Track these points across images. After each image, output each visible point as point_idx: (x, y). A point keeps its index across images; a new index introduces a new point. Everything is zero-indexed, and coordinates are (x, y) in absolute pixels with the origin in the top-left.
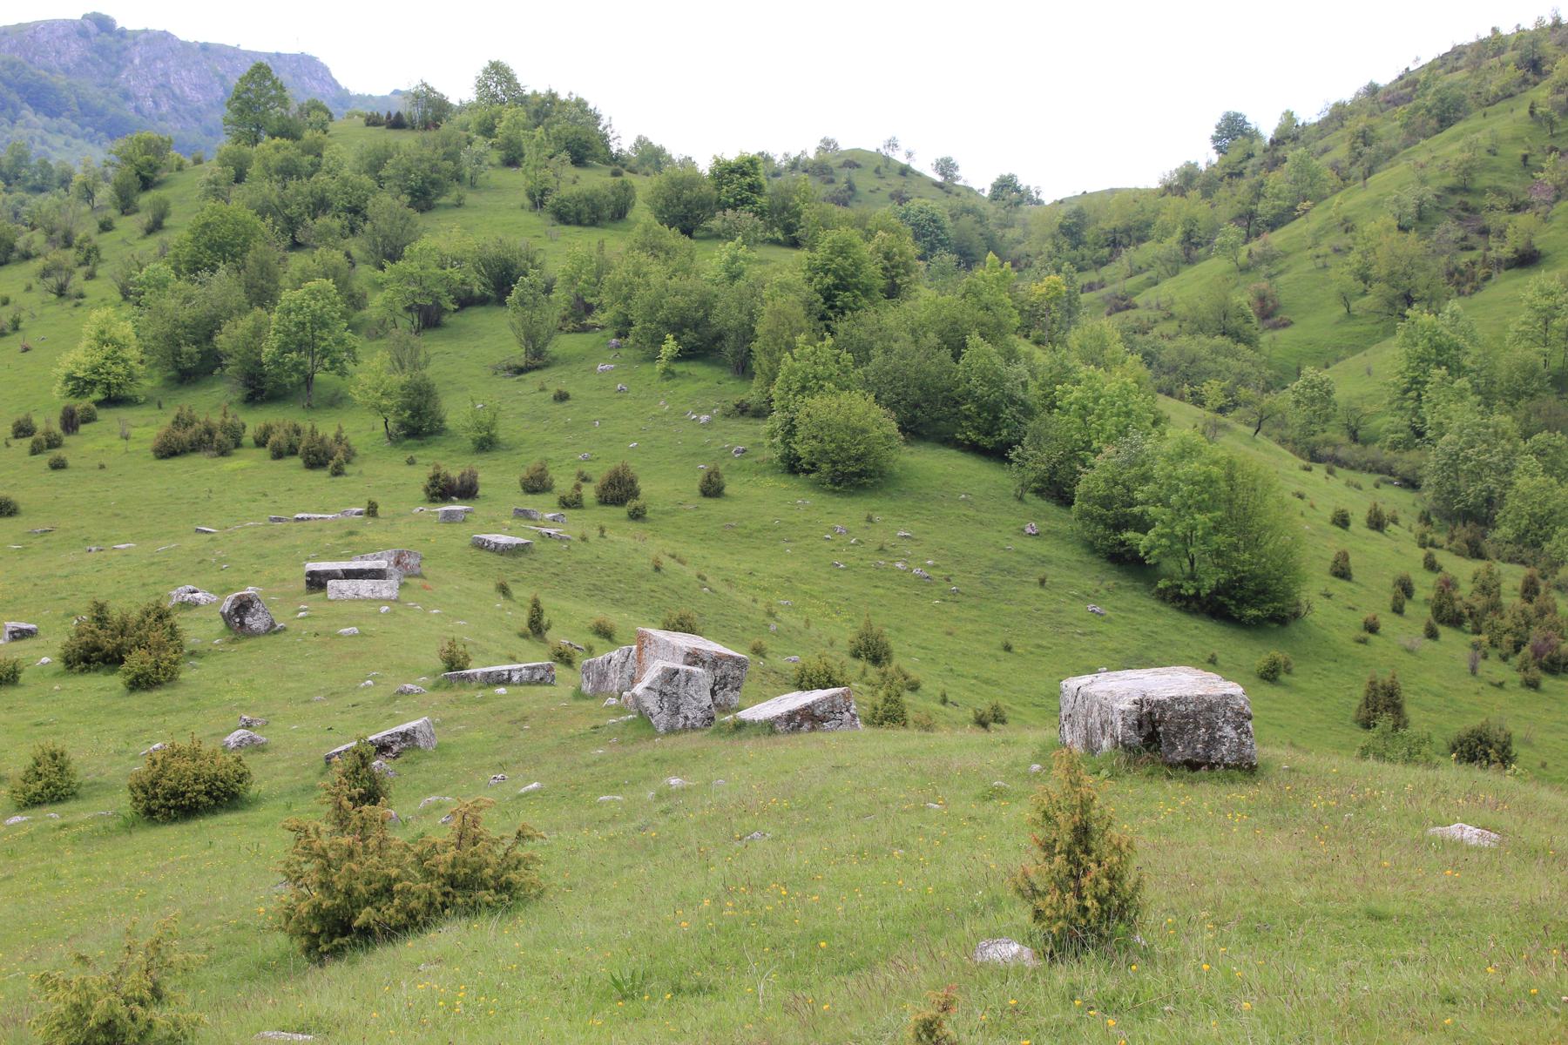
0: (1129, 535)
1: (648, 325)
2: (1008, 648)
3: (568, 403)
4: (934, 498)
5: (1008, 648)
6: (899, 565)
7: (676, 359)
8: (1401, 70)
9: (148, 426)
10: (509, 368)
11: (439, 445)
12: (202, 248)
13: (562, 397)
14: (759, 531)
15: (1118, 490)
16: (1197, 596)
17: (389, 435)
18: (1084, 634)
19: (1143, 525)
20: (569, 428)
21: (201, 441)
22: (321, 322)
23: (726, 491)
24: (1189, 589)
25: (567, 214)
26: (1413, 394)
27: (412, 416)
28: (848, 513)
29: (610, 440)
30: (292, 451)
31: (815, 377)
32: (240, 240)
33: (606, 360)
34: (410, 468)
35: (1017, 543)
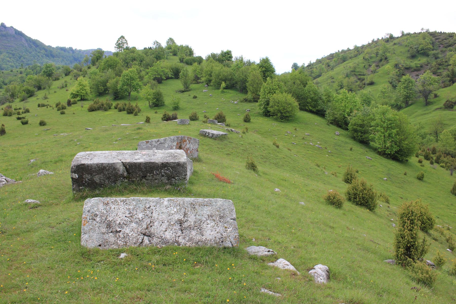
1: (217, 80)
3: (197, 99)
4: (309, 124)
7: (224, 88)
8: (322, 57)
9: (87, 105)
10: (180, 91)
11: (163, 109)
12: (106, 66)
13: (195, 97)
14: (265, 132)
17: (150, 106)
18: (371, 166)
20: (198, 105)
21: (100, 107)
22: (132, 79)
23: (251, 120)
24: (388, 151)
25: (188, 63)
27: (156, 101)
28: (288, 128)
29: (211, 107)
30: (124, 110)
31: (273, 89)
32: (115, 65)
33: (205, 89)
34: (156, 114)
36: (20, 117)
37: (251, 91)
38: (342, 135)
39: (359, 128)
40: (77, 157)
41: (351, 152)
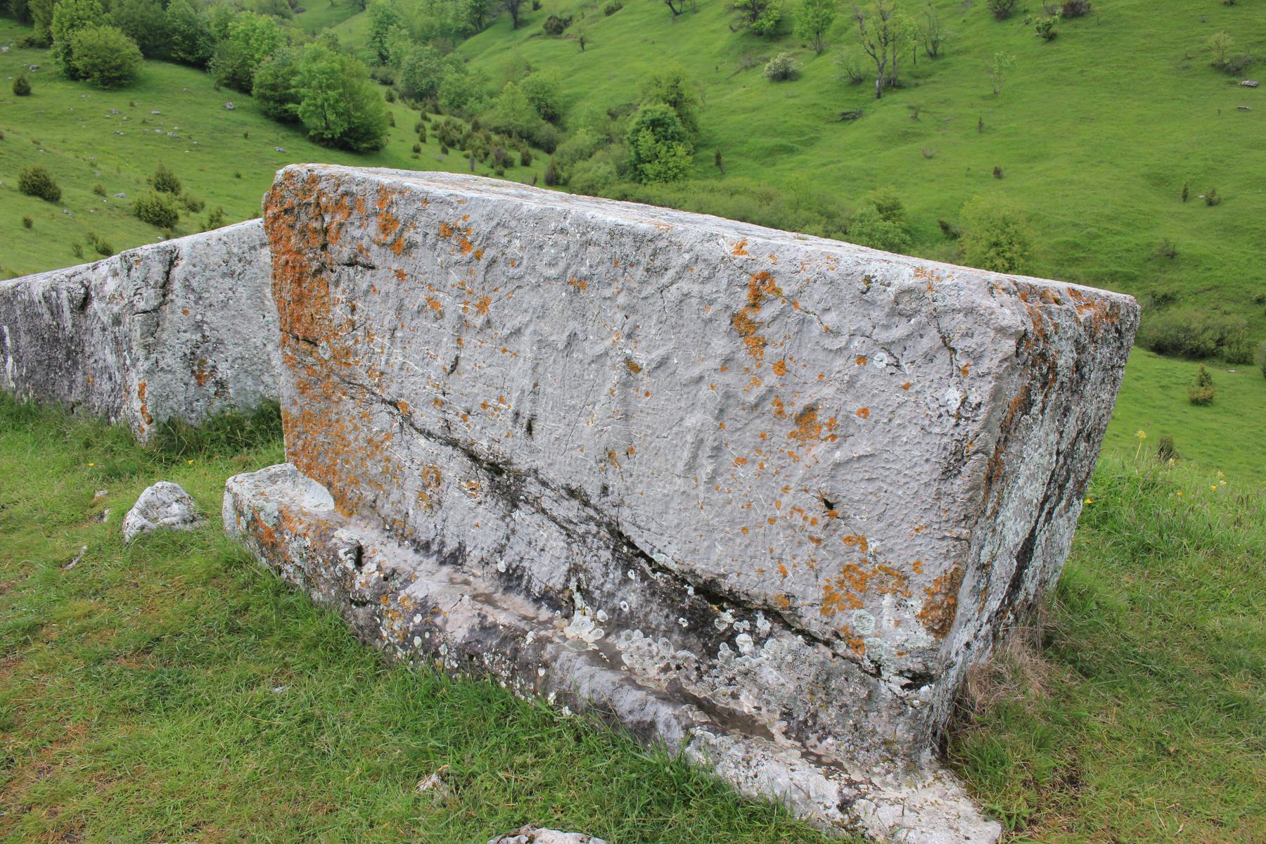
0: (290, 106)
2: (238, 176)
5: (238, 176)
6: (158, 131)
15: (280, 80)
16: (333, 139)
19: (296, 99)
24: (328, 135)
26: (378, 39)
28: (117, 102)
35: (224, 114)
36: (588, 215)
37: (39, 19)
38: (243, 108)
39: (268, 93)
40: (675, 805)
41: (246, 141)
